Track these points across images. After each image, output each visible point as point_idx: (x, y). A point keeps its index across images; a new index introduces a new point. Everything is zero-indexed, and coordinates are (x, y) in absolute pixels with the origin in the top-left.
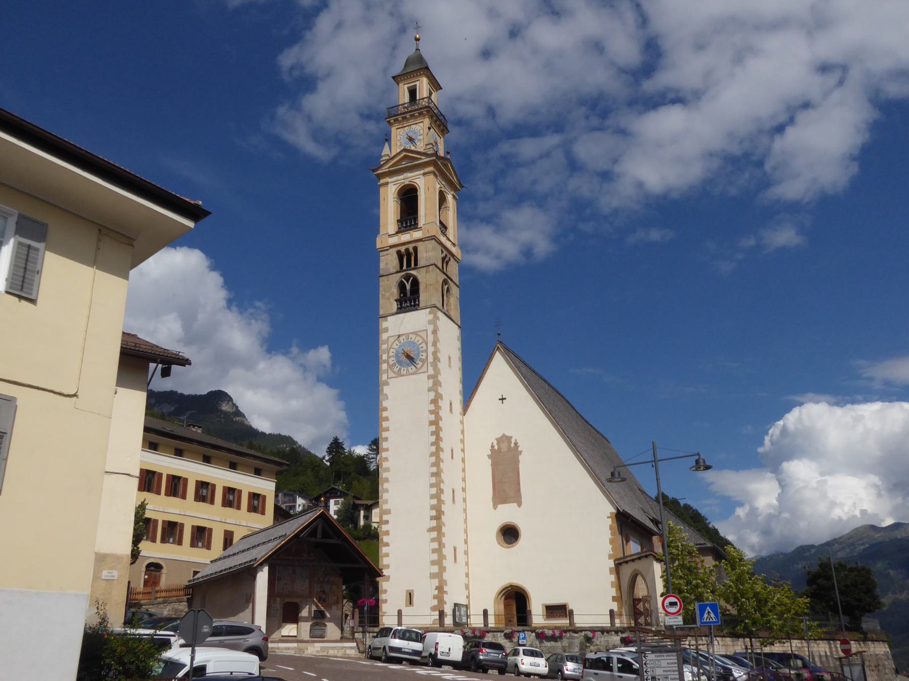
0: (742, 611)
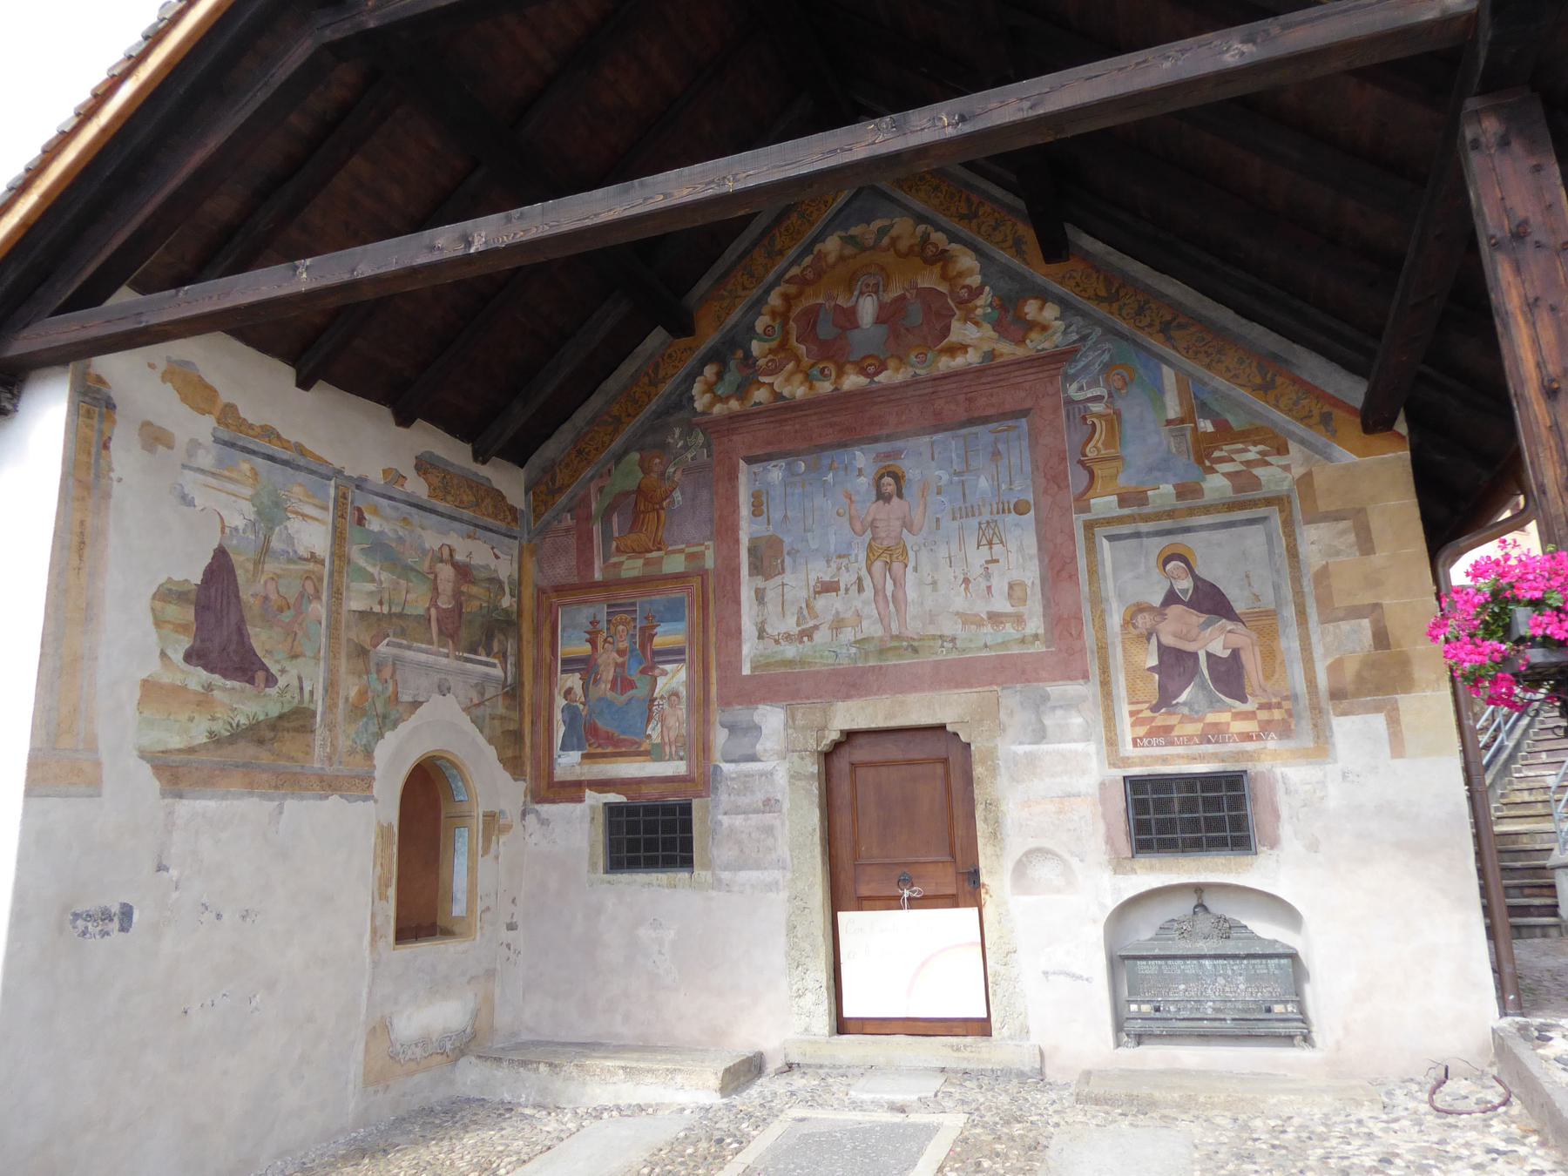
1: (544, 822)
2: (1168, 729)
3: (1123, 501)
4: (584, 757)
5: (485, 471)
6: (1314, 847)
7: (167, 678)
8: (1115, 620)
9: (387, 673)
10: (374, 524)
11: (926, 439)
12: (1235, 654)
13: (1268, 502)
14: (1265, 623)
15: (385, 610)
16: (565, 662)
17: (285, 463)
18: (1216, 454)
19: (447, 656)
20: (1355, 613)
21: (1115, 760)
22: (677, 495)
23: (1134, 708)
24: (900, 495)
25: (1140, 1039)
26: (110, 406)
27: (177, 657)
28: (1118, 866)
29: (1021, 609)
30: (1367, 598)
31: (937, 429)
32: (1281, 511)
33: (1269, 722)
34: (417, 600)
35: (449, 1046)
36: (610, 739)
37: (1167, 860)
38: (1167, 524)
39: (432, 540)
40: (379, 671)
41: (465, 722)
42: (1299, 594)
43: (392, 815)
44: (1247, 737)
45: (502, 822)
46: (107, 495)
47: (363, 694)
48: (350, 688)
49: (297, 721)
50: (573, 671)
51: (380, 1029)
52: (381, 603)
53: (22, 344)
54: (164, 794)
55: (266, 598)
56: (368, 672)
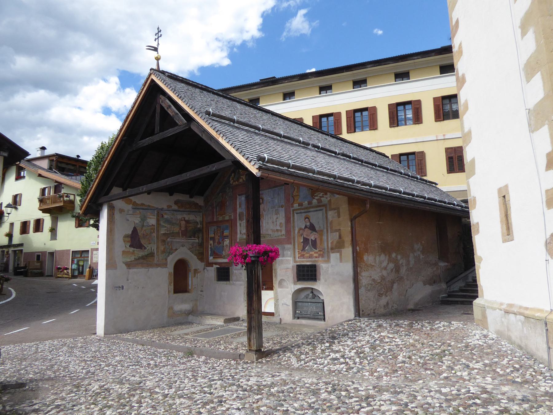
0: (50, 383)
1: (207, 271)
2: (304, 255)
3: (299, 206)
4: (213, 258)
5: (193, 200)
6: (326, 281)
7: (126, 250)
8: (296, 231)
9: (170, 244)
10: (166, 216)
11: (267, 191)
12: (316, 239)
13: (323, 206)
14: (321, 233)
15: (169, 232)
16: (210, 238)
17: (146, 209)
18: (315, 195)
19: (184, 239)
20: (336, 231)
21: (295, 261)
22: (228, 203)
23: (299, 250)
24: (263, 203)
25: (298, 318)
26: (114, 207)
27: (128, 246)
28: (295, 284)
29: (281, 229)
30: (338, 228)
31: (269, 188)
32: (325, 208)
33: (320, 254)
34: (176, 229)
35: (186, 313)
36: (217, 254)
37: (302, 282)
38: (306, 210)
39: (179, 217)
40: (168, 244)
41: (189, 252)
42: (327, 226)
43: (172, 271)
44: (316, 257)
45: (198, 271)
46: (114, 222)
47: (164, 249)
48: (162, 248)
49: (151, 255)
50: (211, 240)
51: (170, 308)
52: (168, 231)
53: (100, 201)
54: (127, 269)
55: (144, 234)
56: (165, 245)
